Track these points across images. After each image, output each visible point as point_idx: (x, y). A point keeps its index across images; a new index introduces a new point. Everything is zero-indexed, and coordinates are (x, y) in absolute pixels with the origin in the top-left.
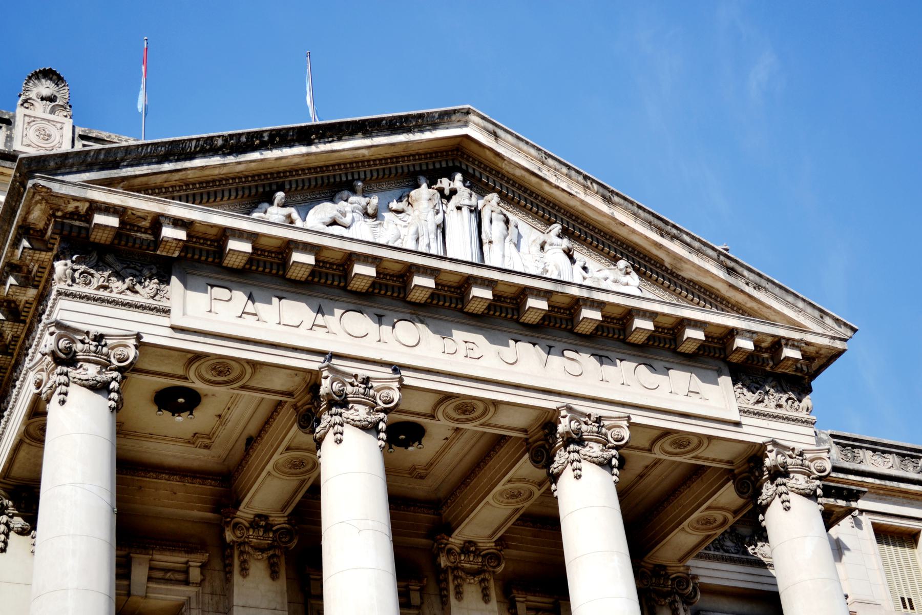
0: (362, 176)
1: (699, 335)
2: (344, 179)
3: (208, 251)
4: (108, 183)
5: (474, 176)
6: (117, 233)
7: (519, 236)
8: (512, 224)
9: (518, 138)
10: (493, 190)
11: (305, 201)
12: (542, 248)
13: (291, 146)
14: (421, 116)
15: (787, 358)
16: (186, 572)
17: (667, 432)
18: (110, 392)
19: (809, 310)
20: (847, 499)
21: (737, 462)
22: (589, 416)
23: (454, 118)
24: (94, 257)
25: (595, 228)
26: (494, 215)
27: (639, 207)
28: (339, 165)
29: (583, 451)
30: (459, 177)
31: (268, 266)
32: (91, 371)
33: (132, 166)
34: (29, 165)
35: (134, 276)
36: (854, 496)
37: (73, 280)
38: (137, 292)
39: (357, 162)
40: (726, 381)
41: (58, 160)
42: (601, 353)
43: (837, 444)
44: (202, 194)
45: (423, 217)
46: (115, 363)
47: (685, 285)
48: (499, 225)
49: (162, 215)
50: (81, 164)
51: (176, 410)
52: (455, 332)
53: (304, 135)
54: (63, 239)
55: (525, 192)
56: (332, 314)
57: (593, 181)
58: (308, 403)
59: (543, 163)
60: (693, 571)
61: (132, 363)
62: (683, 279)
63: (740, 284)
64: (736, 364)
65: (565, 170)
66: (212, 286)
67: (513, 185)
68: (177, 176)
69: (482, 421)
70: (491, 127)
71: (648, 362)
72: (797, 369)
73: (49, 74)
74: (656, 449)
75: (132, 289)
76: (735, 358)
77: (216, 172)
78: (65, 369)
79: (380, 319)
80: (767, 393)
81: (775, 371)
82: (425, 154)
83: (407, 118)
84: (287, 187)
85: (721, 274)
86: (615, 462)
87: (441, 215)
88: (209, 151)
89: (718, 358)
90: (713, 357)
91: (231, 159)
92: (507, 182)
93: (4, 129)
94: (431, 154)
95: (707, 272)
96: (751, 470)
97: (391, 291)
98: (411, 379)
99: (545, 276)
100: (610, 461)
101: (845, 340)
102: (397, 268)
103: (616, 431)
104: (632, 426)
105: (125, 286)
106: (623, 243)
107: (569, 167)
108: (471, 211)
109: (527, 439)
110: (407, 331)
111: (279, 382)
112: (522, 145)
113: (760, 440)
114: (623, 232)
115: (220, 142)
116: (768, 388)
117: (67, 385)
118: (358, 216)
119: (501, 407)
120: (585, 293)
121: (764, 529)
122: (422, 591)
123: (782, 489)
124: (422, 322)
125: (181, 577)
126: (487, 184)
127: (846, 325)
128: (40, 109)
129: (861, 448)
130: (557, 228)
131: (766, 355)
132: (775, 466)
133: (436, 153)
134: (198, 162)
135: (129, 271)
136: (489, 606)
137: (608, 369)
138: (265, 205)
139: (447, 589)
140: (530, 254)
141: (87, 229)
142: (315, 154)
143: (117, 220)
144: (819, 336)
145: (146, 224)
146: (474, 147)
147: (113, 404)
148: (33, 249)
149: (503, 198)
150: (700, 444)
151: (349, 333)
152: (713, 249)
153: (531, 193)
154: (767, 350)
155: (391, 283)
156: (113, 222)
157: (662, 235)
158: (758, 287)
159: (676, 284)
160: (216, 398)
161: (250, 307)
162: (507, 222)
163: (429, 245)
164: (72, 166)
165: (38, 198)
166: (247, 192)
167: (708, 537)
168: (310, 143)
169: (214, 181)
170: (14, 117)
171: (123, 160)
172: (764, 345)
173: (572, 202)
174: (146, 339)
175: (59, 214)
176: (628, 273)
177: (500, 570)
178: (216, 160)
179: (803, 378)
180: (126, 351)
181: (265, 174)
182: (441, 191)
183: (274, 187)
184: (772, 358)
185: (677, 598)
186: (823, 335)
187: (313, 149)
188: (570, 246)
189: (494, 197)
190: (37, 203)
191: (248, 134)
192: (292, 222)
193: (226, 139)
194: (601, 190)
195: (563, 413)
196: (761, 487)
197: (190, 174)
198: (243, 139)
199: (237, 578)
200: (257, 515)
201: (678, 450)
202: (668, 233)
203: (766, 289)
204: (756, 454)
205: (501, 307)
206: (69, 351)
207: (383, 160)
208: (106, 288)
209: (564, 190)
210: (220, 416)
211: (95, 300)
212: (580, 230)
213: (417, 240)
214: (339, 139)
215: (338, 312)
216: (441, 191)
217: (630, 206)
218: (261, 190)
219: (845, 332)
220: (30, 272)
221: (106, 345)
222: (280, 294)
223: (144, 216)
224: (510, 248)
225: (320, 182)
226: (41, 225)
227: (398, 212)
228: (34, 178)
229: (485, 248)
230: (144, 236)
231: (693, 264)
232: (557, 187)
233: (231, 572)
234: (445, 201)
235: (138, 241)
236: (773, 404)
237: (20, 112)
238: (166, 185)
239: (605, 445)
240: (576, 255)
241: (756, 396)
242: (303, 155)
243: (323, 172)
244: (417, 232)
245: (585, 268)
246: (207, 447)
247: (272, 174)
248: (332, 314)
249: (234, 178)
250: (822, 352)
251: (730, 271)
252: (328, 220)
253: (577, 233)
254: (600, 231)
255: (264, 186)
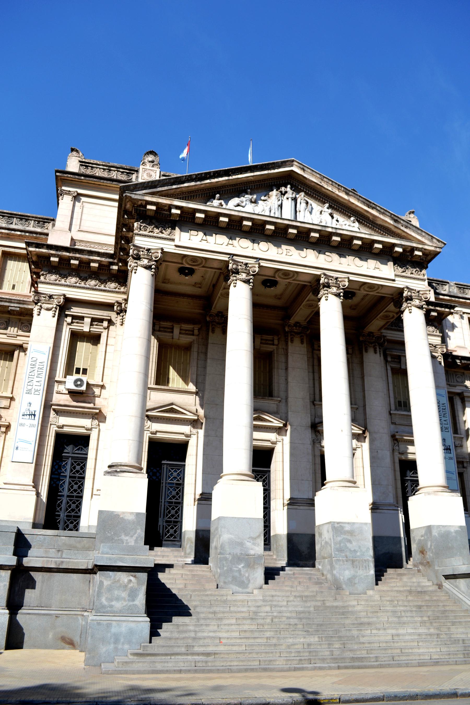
0: (251, 187)
1: (380, 246)
2: (243, 189)
3: (189, 217)
4: (153, 194)
5: (295, 186)
6: (156, 211)
7: (312, 208)
8: (309, 204)
9: (312, 170)
10: (303, 191)
11: (229, 197)
12: (321, 213)
13: (222, 177)
14: (274, 163)
15: (416, 255)
16: (193, 331)
17: (365, 283)
18: (152, 269)
19: (427, 236)
20: (450, 309)
21: (394, 295)
22: (333, 277)
23: (287, 163)
24: (148, 220)
25: (342, 205)
26: (302, 201)
27: (360, 196)
28: (242, 183)
29: (329, 290)
30: (289, 186)
31: (212, 222)
32: (145, 262)
33: (161, 187)
34: (124, 188)
35: (162, 227)
36: (453, 307)
37: (140, 229)
38: (163, 233)
39: (249, 182)
40: (391, 264)
41: (134, 186)
42: (340, 253)
43: (457, 287)
44: (188, 196)
45: (273, 202)
46: (154, 259)
47: (378, 227)
48: (304, 205)
49: (171, 205)
50: (142, 187)
51: (186, 275)
52: (282, 246)
53: (227, 173)
54: (138, 215)
55: (315, 191)
56: (236, 240)
57: (342, 187)
58: (224, 273)
59: (322, 180)
60: (385, 334)
61: (159, 259)
62: (377, 224)
63: (400, 226)
64: (396, 257)
65: (330, 183)
66: (191, 230)
67: (311, 189)
68: (179, 190)
69: (293, 279)
70: (302, 166)
71: (359, 256)
72: (421, 259)
73: (152, 153)
74: (362, 289)
75: (161, 232)
76: (395, 255)
77: (194, 188)
78: (136, 261)
79: (253, 241)
80: (407, 268)
81: (408, 259)
82: (276, 178)
83: (268, 164)
84: (221, 192)
85: (392, 222)
86: (342, 294)
87: (280, 201)
88: (190, 180)
89: (389, 255)
90: (387, 254)
91: (199, 183)
92: (309, 188)
93: (135, 174)
94: (278, 178)
95: (386, 222)
96: (398, 298)
97: (257, 231)
98: (263, 264)
99: (320, 224)
100: (340, 294)
101: (441, 248)
102: (260, 222)
103: (343, 283)
104: (350, 281)
105: (159, 231)
106: (353, 211)
107: (332, 182)
108: (292, 200)
109: (311, 286)
110: (264, 245)
111: (216, 265)
112: (314, 173)
113: (402, 287)
114: (354, 206)
115: (194, 177)
116: (408, 266)
117: (137, 267)
118: (248, 202)
119: (299, 274)
120: (334, 231)
121: (402, 320)
122: (278, 340)
123: (409, 305)
124: (270, 242)
125: (191, 333)
126: (300, 189)
127: (442, 242)
128: (148, 166)
129: (467, 289)
130: (327, 205)
131: (408, 254)
132: (407, 296)
133: (281, 177)
134: (186, 185)
135: (161, 225)
136: (303, 345)
137: (343, 260)
138: (212, 199)
139: (288, 339)
140: (316, 216)
141: (146, 211)
142: (231, 179)
143: (147, 208)
144: (430, 246)
145: (166, 208)
146: (296, 175)
147: (152, 273)
148: (128, 218)
149: (307, 194)
150: (378, 288)
151: (242, 247)
152: (389, 212)
153: (318, 192)
154: (409, 252)
155: (258, 228)
156: (154, 208)
157: (369, 207)
158: (406, 227)
159: (374, 226)
160: (200, 271)
161: (204, 238)
162: (307, 203)
163: (275, 213)
164: (139, 188)
165: (128, 200)
166: (206, 195)
167: (388, 322)
168: (229, 176)
169: (193, 191)
170: (139, 169)
171: (158, 185)
172: (408, 250)
173: (334, 195)
174: (165, 250)
175: (136, 205)
176: (354, 222)
177: (308, 332)
178: (193, 184)
179: (423, 263)
180: (157, 254)
181: (213, 188)
182: (281, 192)
183: (216, 193)
184: (411, 255)
185: (377, 344)
186: (432, 246)
187: (231, 178)
188: (332, 212)
189: (302, 194)
190: (128, 202)
191: (205, 173)
192: (222, 206)
193: (197, 175)
194: (345, 190)
195: (322, 276)
196: (402, 304)
197: (184, 189)
198: (203, 175)
199: (210, 334)
200: (218, 312)
201: (370, 290)
202: (371, 206)
203: (410, 228)
204: (401, 291)
205: (301, 236)
206: (137, 255)
207: (259, 181)
208: (152, 232)
209: (330, 191)
210: (202, 277)
211: (148, 236)
212: (337, 206)
213: (270, 211)
214: (241, 174)
215: (238, 239)
216: (281, 192)
217: (356, 196)
218: (211, 194)
219: (440, 245)
220: (130, 226)
221: (151, 252)
222: (216, 233)
223: (166, 205)
224: (307, 213)
225: (234, 190)
226: (131, 210)
227: (264, 200)
228: (125, 193)
229: (298, 213)
230: (166, 213)
231: (381, 219)
232: (327, 189)
233: (209, 332)
234: (283, 196)
235: (164, 215)
236: (409, 273)
237: (141, 167)
238: (175, 193)
239: (338, 288)
240: (335, 215)
241: (403, 270)
242: (226, 180)
243: (235, 186)
244: (270, 208)
245: (337, 221)
246: (200, 288)
247: (215, 188)
248: (236, 240)
249: (201, 190)
250: (432, 252)
251: (396, 221)
252: (236, 204)
253: (335, 207)
254: (345, 206)
255: (212, 192)
